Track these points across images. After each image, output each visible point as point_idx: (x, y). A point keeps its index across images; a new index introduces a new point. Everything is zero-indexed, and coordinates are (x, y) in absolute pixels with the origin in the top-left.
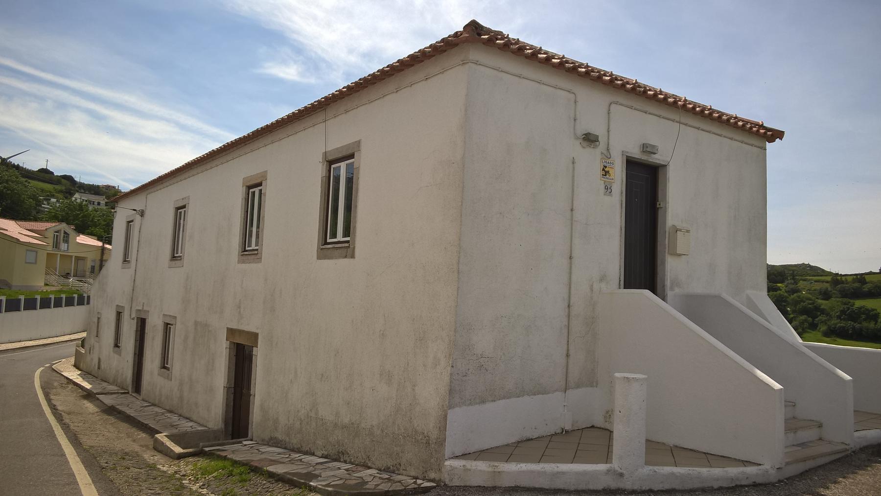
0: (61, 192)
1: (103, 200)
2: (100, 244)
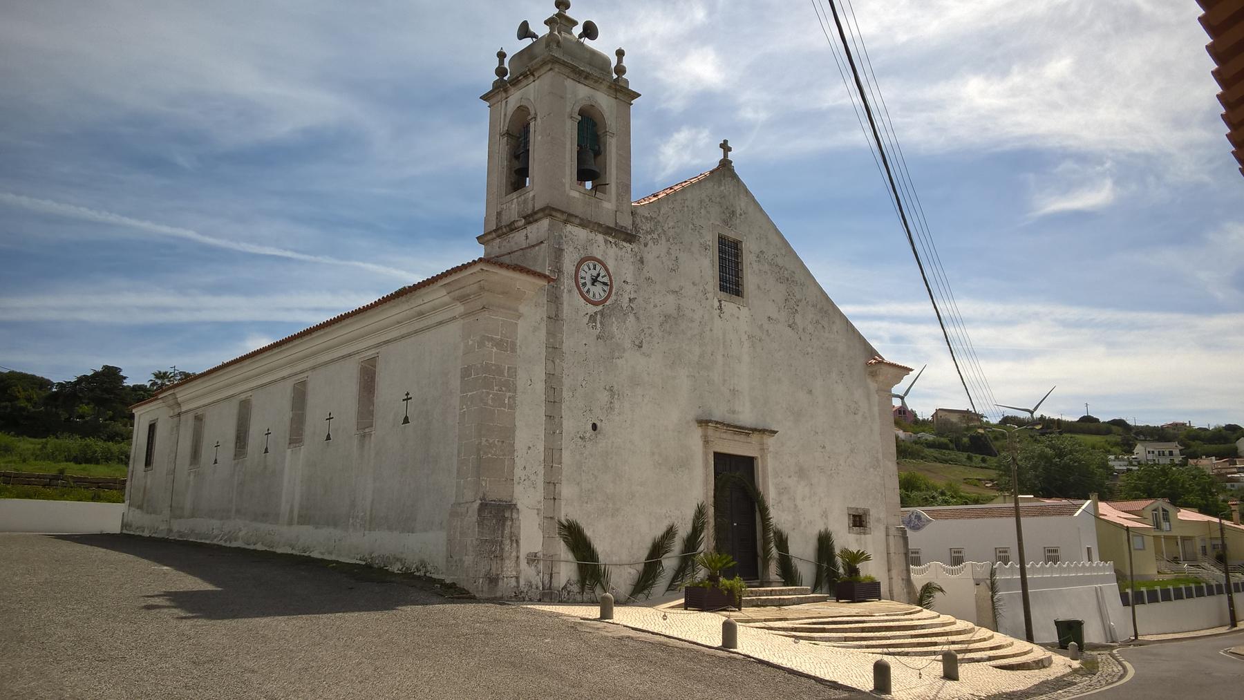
0: (1116, 444)
1: (1175, 447)
2: (1216, 520)
